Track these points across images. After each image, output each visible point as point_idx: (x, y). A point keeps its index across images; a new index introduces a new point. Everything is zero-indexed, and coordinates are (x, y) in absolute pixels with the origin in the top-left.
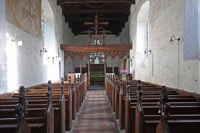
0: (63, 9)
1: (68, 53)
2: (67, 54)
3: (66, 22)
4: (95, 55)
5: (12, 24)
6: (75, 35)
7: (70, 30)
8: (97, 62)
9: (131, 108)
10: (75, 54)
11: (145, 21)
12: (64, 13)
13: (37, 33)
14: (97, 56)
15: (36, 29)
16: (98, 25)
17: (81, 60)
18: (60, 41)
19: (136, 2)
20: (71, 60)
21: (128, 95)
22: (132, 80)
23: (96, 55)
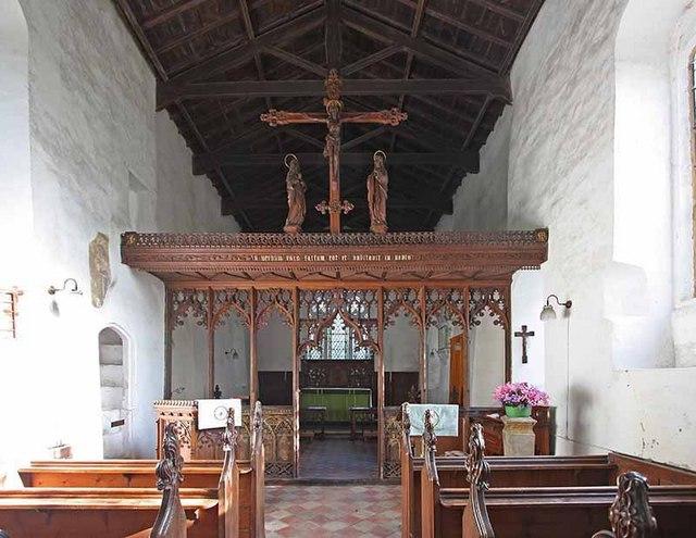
1: (185, 291)
2: (181, 297)
8: (339, 343)
9: (441, 505)
10: (222, 297)
11: (669, 53)
12: (167, 100)
16: (344, 127)
17: (256, 329)
20: (203, 327)
21: (432, 461)
22: (552, 453)
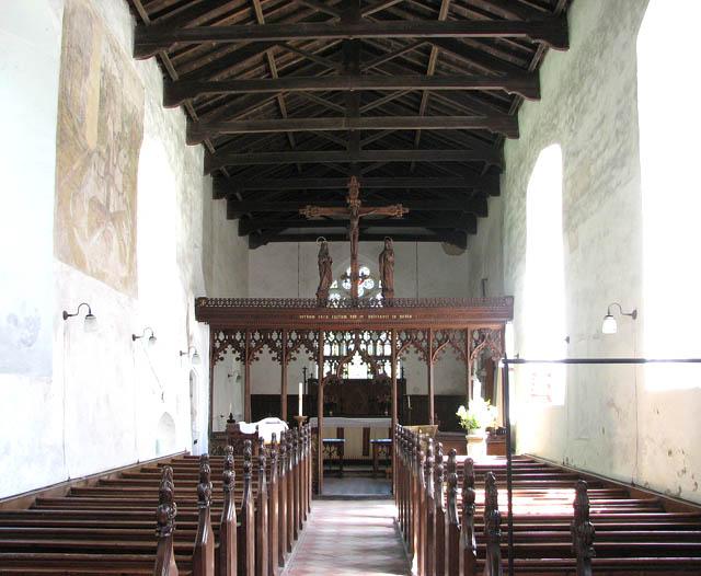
0: (139, 20)
3: (217, 196)
4: (348, 343)
5: (66, 263)
6: (254, 244)
7: (234, 225)
8: (357, 370)
12: (211, 166)
13: (124, 273)
14: (357, 348)
15: (123, 261)
18: (194, 288)
19: (583, 22)
23: (352, 347)
